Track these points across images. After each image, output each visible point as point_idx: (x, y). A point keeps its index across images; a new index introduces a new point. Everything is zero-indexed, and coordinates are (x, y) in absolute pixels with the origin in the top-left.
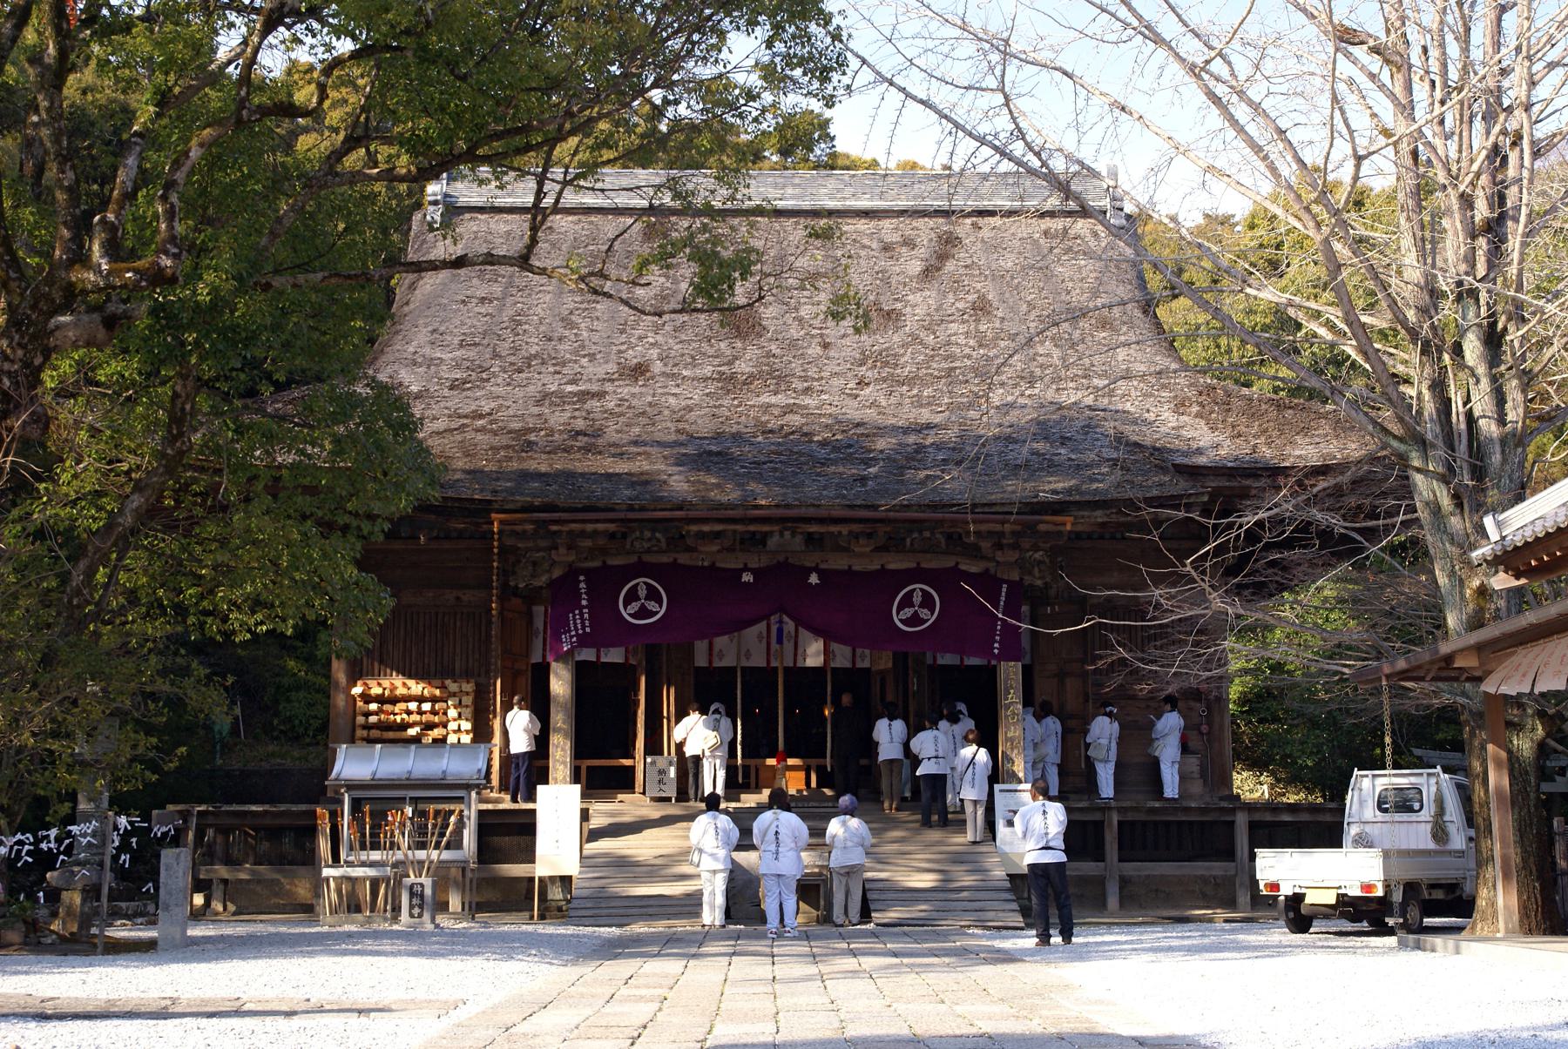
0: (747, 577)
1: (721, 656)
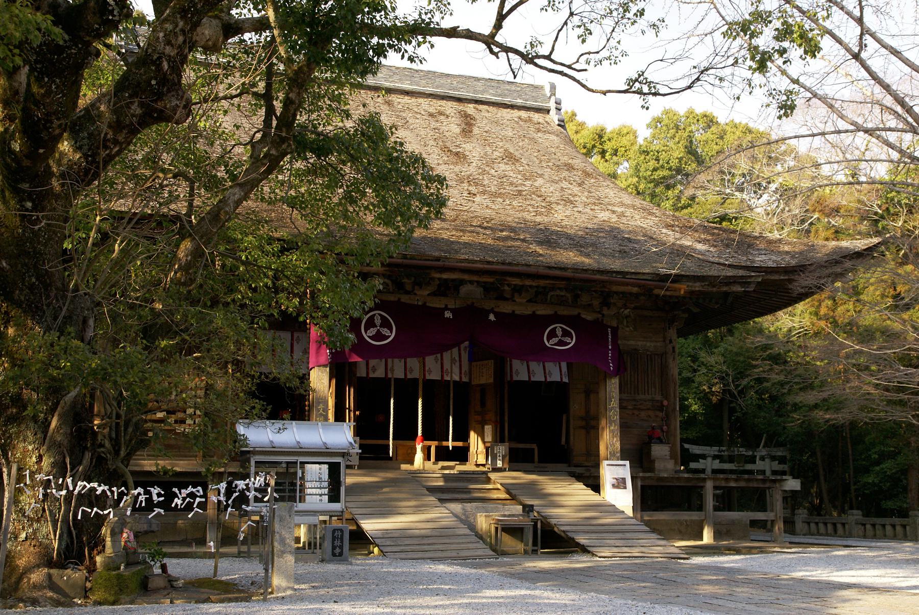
0: (448, 314)
1: (374, 370)
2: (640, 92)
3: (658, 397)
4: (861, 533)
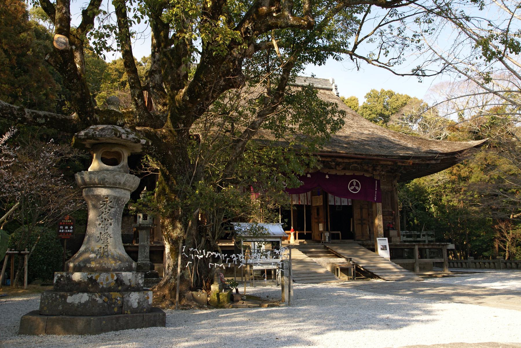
2: (418, 75)
3: (390, 210)
4: (474, 266)
